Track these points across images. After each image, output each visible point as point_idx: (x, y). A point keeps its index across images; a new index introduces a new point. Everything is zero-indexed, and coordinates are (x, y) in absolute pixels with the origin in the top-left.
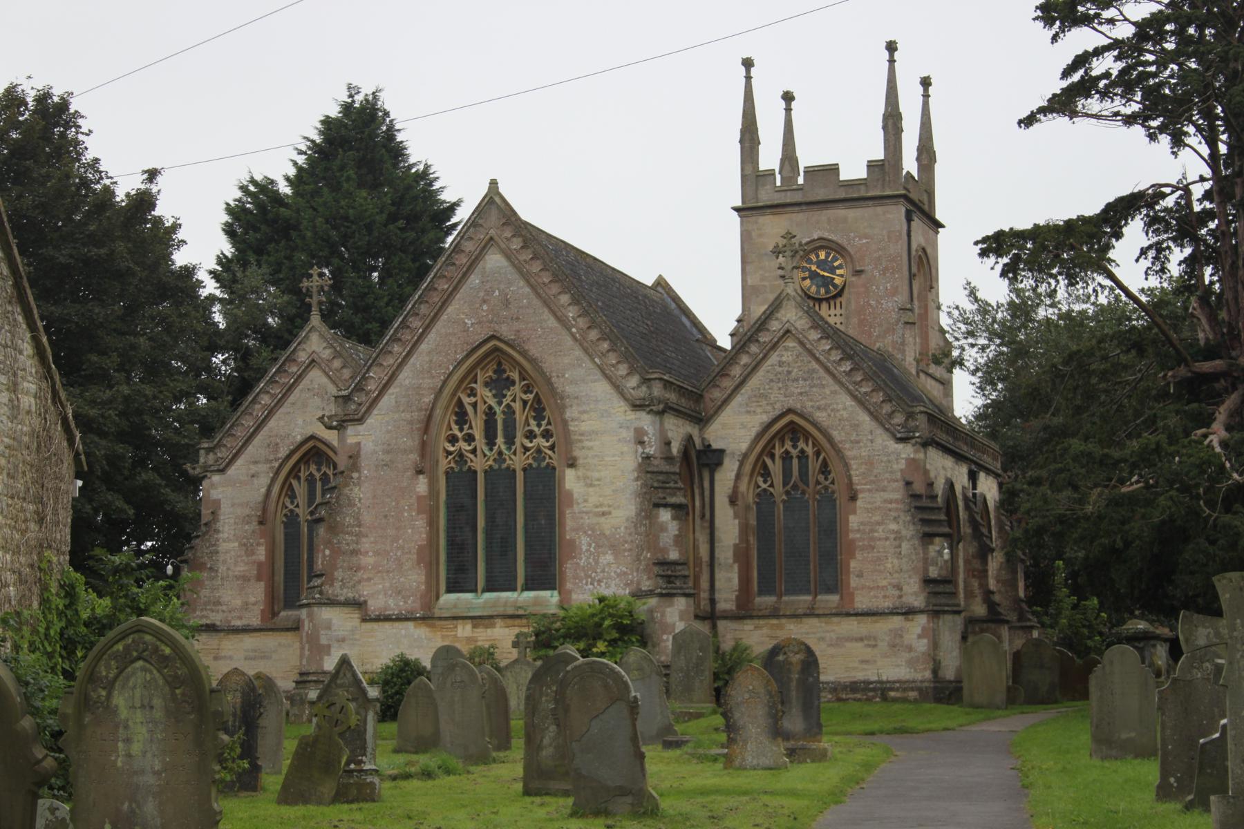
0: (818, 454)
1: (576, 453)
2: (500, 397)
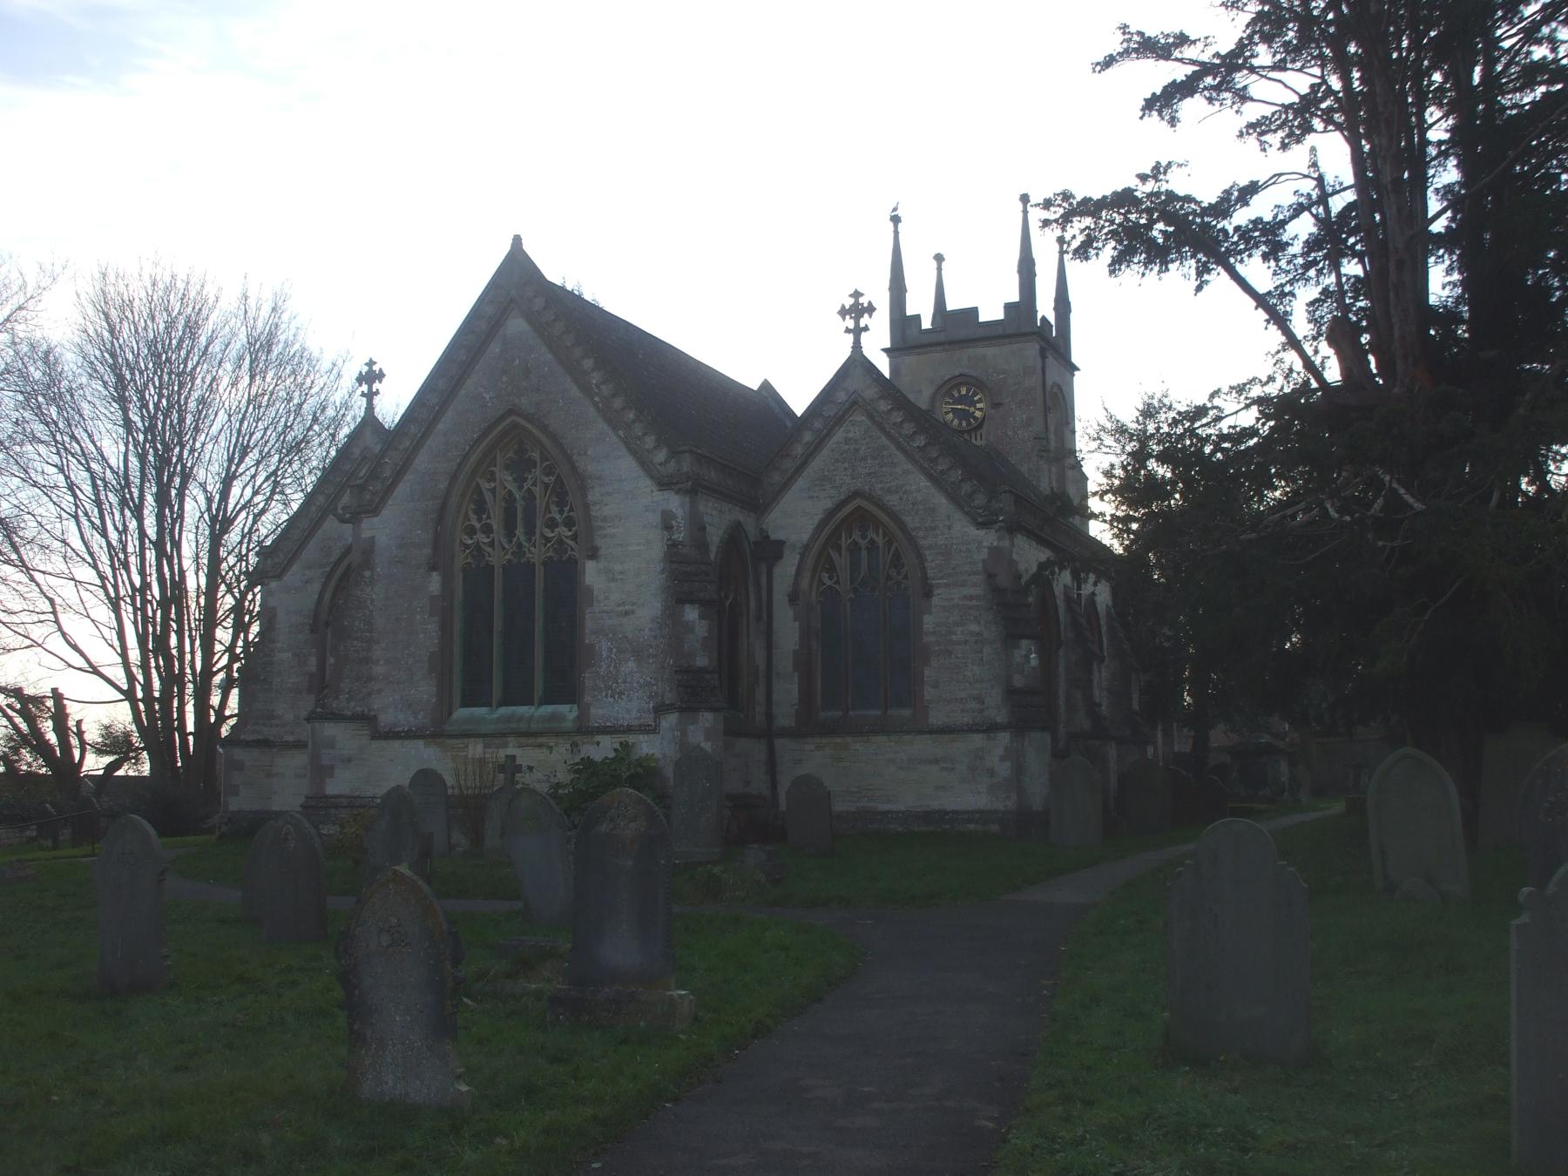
0: (889, 543)
1: (599, 542)
2: (520, 480)
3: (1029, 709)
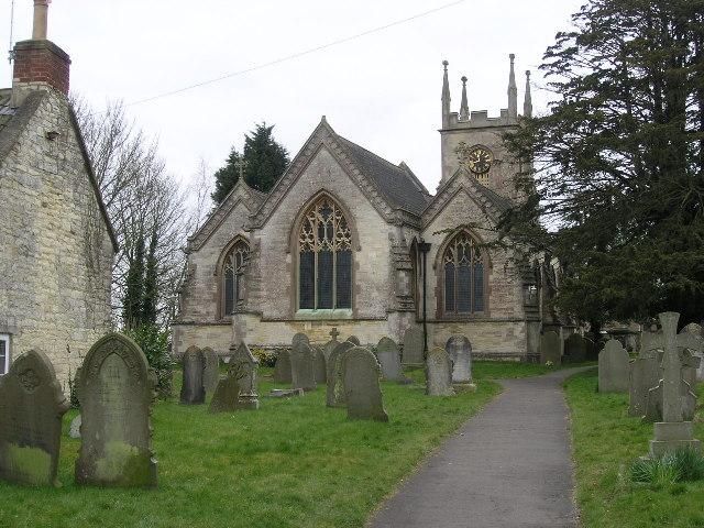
2: (325, 218)
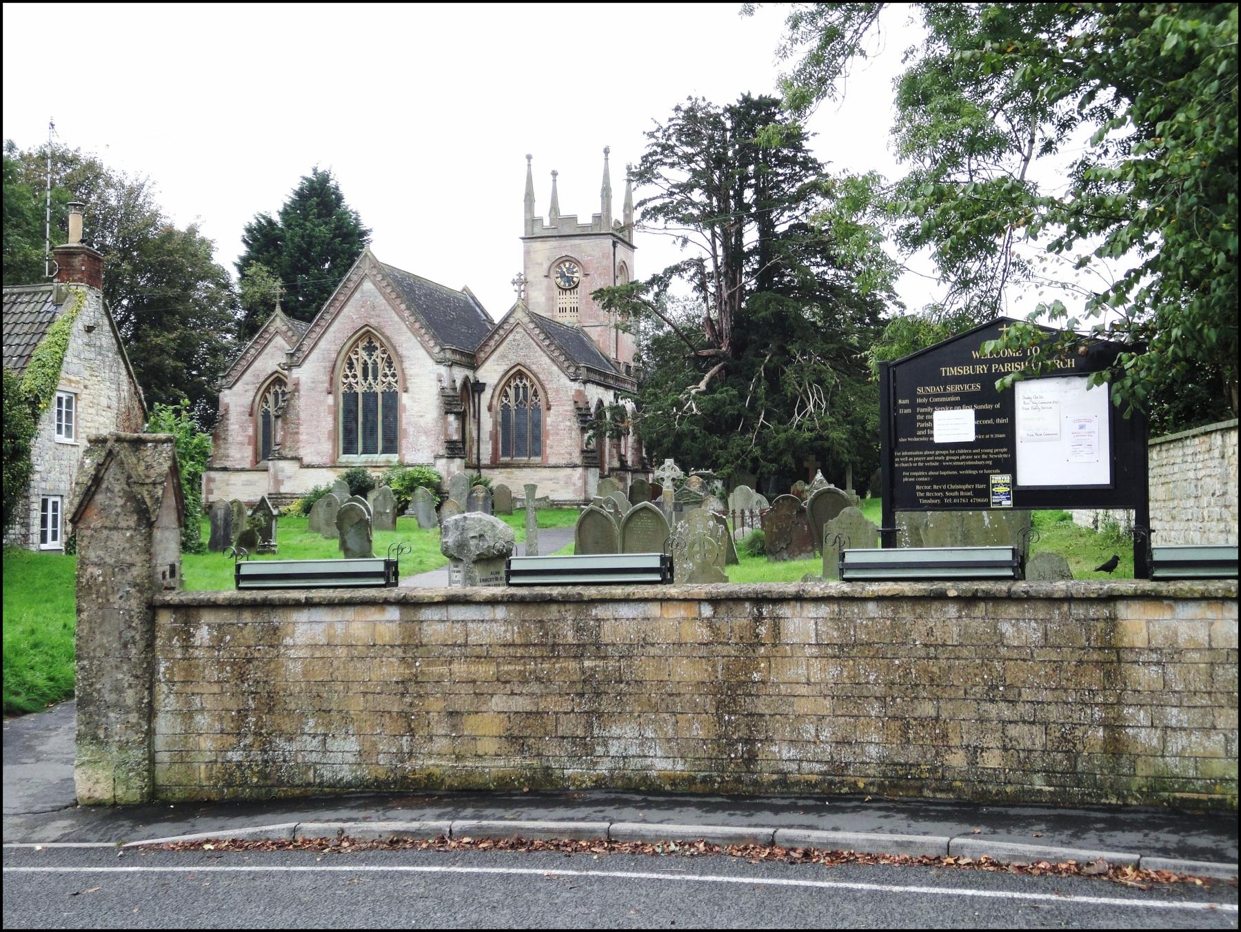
2: (370, 355)
3: (591, 459)
